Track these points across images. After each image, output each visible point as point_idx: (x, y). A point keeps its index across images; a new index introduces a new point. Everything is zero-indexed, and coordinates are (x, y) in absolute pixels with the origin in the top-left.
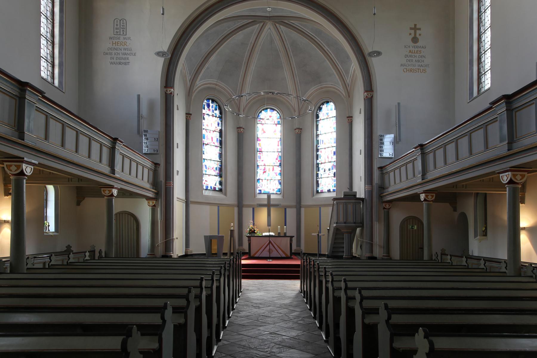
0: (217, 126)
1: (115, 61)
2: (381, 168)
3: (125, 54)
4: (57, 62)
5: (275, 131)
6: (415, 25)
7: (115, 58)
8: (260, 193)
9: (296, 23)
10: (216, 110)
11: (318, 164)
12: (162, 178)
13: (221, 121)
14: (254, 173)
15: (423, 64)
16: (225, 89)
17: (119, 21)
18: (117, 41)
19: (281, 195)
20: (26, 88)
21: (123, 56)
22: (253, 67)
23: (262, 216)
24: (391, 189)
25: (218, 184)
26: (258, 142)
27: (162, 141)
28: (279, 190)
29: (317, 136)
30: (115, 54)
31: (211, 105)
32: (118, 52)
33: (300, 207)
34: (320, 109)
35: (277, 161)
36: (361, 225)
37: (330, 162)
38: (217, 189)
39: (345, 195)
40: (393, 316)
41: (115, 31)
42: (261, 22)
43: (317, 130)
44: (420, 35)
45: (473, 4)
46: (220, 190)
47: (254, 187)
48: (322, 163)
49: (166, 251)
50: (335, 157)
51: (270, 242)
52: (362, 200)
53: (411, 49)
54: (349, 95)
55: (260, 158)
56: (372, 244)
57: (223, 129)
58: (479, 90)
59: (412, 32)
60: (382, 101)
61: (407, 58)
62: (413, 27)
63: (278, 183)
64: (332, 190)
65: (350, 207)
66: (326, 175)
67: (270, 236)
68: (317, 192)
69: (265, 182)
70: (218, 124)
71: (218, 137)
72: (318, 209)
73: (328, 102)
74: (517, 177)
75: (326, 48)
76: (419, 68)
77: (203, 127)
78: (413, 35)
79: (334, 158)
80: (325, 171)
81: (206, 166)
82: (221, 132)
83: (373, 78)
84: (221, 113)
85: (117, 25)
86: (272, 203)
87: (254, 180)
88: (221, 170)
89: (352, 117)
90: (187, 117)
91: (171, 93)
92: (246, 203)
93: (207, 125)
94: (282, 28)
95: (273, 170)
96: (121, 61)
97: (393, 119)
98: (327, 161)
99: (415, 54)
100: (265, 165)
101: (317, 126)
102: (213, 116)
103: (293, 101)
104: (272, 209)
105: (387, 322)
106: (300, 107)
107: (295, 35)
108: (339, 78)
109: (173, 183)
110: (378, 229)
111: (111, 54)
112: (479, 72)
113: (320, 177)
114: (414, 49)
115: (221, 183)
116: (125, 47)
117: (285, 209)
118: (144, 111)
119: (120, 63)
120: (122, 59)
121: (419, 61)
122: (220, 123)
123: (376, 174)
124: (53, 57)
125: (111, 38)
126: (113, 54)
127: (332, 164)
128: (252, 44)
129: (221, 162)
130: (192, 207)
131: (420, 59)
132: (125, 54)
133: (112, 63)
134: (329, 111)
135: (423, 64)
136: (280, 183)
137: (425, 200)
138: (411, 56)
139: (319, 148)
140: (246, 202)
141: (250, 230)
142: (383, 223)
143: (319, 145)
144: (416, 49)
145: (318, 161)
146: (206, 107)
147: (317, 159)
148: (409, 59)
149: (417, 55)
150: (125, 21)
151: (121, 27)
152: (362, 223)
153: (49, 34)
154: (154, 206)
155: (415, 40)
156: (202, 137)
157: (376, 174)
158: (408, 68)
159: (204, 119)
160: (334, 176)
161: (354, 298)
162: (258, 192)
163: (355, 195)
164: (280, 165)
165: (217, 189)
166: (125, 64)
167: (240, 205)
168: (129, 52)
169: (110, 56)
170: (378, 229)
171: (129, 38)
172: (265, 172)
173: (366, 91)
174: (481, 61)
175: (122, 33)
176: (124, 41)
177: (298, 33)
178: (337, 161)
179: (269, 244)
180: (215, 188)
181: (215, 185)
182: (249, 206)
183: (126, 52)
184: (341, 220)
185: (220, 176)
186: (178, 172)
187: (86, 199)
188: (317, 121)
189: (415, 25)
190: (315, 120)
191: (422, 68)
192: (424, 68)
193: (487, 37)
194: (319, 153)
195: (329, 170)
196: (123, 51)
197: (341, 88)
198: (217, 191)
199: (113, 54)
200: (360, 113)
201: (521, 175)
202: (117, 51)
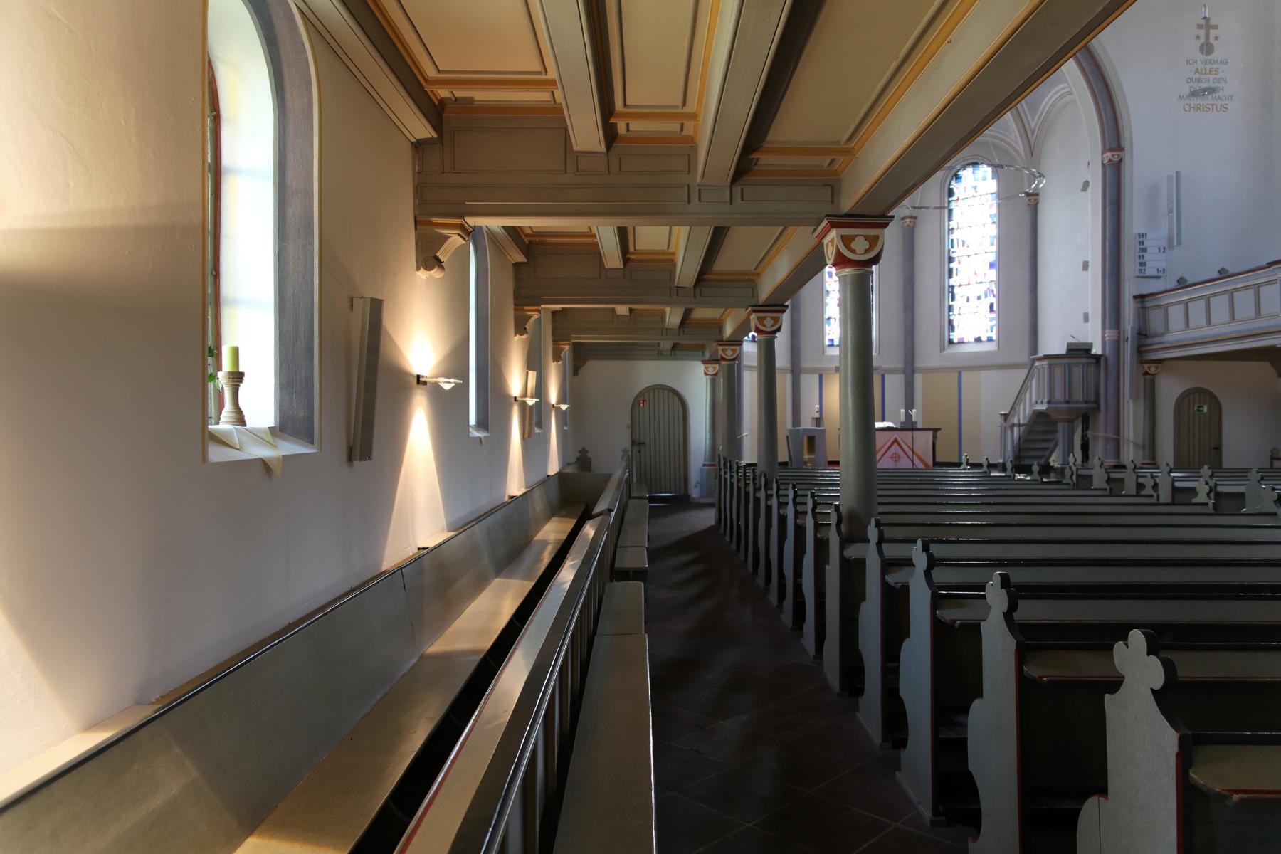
2: (1141, 298)
24: (1170, 338)
29: (951, 230)
33: (913, 372)
39: (1069, 350)
40: (1021, 603)
44: (1216, 38)
51: (896, 441)
53: (1200, 66)
56: (1118, 441)
59: (1202, 32)
60: (1144, 167)
64: (984, 339)
65: (1077, 372)
67: (889, 429)
68: (951, 342)
72: (956, 375)
73: (975, 164)
74: (853, 245)
78: (1202, 40)
79: (993, 274)
83: (1124, 124)
105: (1008, 616)
110: (1132, 416)
113: (956, 310)
127: (984, 287)
139: (953, 255)
140: (806, 363)
142: (1142, 402)
144: (1208, 67)
145: (952, 282)
147: (950, 276)
149: (1211, 77)
155: (1207, 48)
161: (908, 563)
162: (827, 343)
170: (1132, 416)
182: (812, 371)
184: (1059, 395)
187: (589, 362)
194: (952, 265)
195: (979, 298)
201: (866, 237)
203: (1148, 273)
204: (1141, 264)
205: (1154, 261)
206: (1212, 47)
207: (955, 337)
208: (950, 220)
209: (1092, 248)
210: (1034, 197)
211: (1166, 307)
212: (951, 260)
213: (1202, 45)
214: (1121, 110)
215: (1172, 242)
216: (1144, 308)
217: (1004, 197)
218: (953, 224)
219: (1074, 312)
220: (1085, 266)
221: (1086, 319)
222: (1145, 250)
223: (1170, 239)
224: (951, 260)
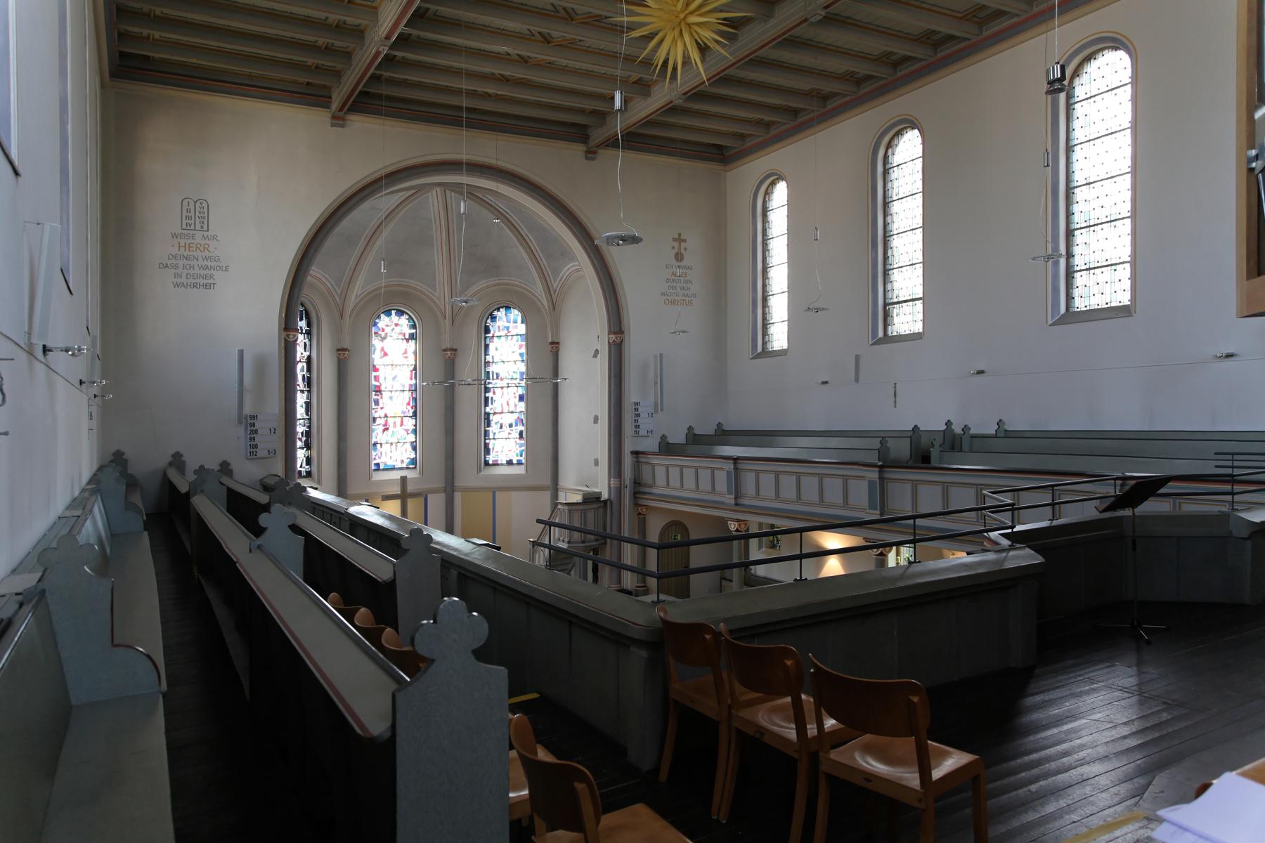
1: (184, 280)
2: (636, 453)
5: (406, 352)
7: (184, 276)
9: (491, 199)
14: (369, 432)
18: (188, 242)
21: (202, 272)
26: (374, 374)
27: (281, 431)
28: (413, 461)
29: (487, 363)
32: (192, 263)
41: (185, 222)
55: (377, 403)
58: (764, 343)
59: (676, 244)
65: (590, 515)
68: (487, 463)
69: (386, 448)
73: (507, 308)
75: (525, 231)
85: (188, 211)
86: (410, 488)
87: (369, 445)
98: (506, 410)
101: (487, 346)
111: (176, 267)
112: (764, 319)
116: (207, 253)
123: (628, 461)
125: (174, 236)
127: (515, 416)
133: (177, 285)
136: (414, 448)
145: (488, 409)
147: (486, 405)
150: (205, 204)
151: (196, 216)
155: (679, 257)
157: (628, 461)
164: (415, 414)
166: (206, 286)
168: (214, 264)
169: (173, 271)
171: (215, 238)
175: (198, 227)
176: (203, 242)
183: (209, 263)
194: (490, 395)
196: (201, 262)
197: (539, 290)
206: (682, 256)
207: (491, 459)
208: (486, 354)
209: (601, 407)
210: (555, 345)
211: (653, 466)
212: (487, 390)
215: (658, 407)
216: (638, 462)
217: (529, 338)
218: (489, 358)
219: (586, 467)
220: (596, 420)
221: (596, 463)
222: (638, 415)
223: (656, 404)
224: (487, 390)
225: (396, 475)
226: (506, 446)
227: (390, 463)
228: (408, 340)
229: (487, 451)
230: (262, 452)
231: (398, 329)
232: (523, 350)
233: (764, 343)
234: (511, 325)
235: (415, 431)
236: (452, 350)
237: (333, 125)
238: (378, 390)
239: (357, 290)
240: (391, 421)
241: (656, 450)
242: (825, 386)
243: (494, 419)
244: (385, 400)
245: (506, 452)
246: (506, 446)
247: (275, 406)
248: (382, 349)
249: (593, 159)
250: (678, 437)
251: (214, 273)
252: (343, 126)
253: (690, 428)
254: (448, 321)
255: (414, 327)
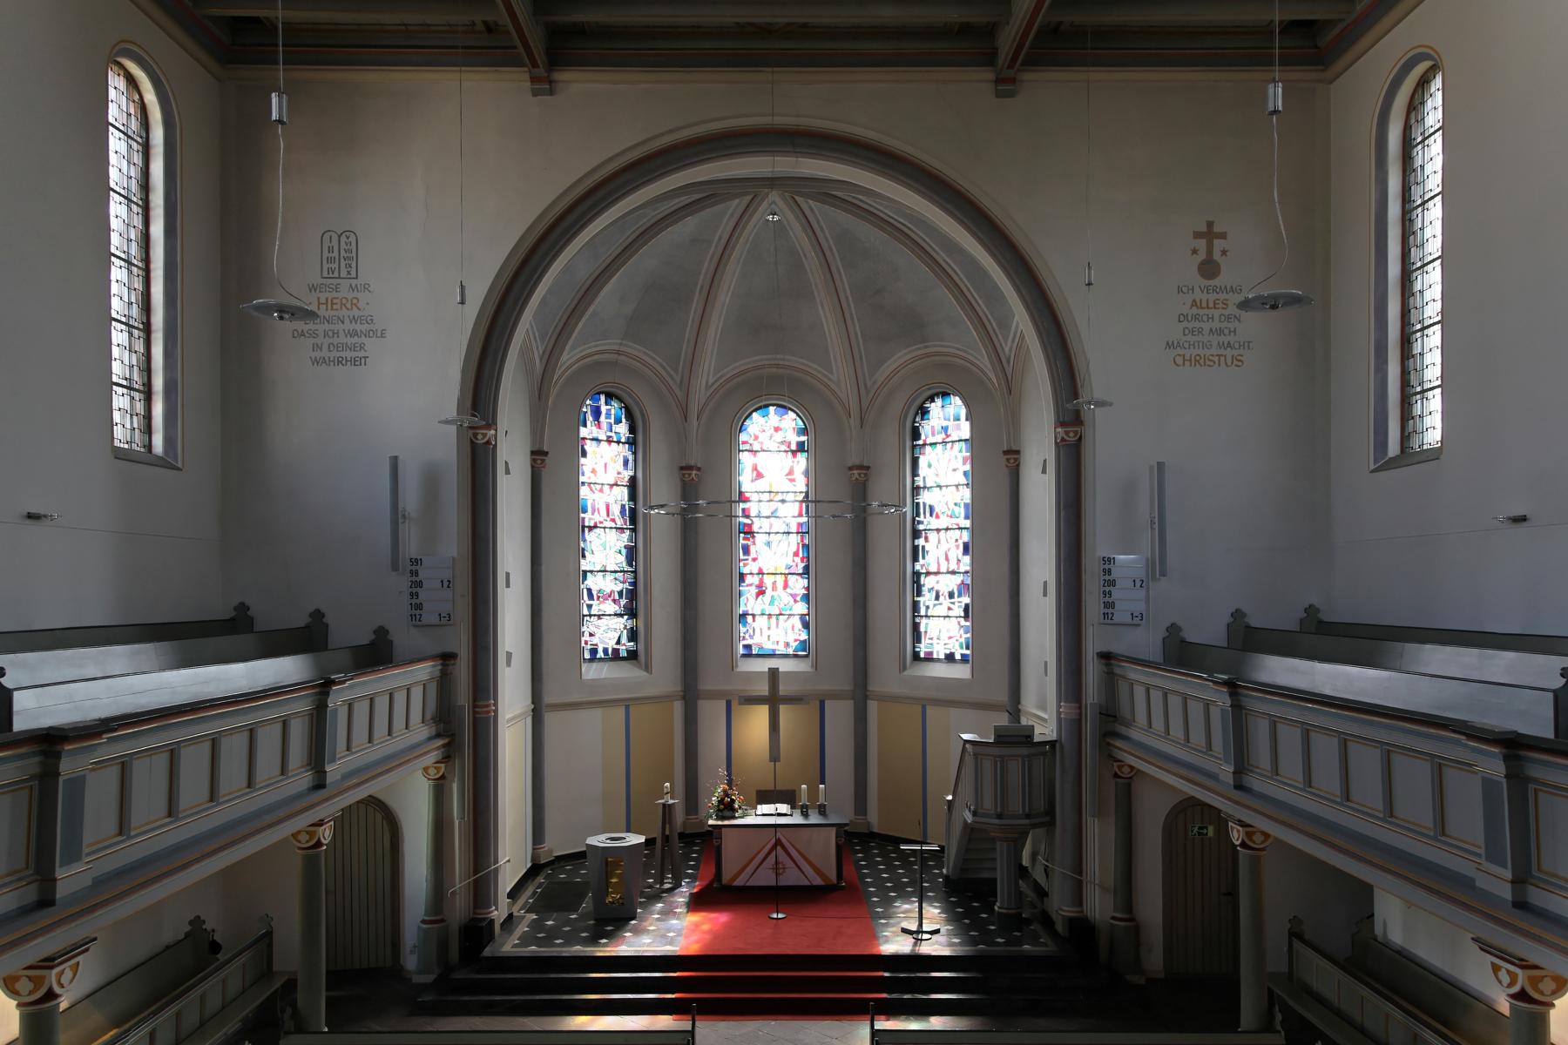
0: (621, 468)
1: (325, 353)
2: (1106, 657)
3: (355, 334)
4: (158, 383)
5: (791, 472)
6: (1210, 224)
7: (325, 347)
8: (748, 655)
10: (618, 421)
11: (917, 575)
12: (463, 696)
13: (635, 453)
14: (732, 597)
15: (1232, 339)
16: (644, 363)
17: (335, 237)
18: (330, 296)
19: (809, 661)
20: (58, 748)
21: (350, 341)
22: (725, 298)
23: (755, 726)
25: (624, 640)
27: (463, 586)
28: (804, 645)
29: (916, 490)
30: (326, 335)
31: (604, 409)
33: (866, 698)
34: (924, 412)
35: (798, 560)
36: (1047, 819)
37: (953, 573)
38: (623, 654)
42: (747, 193)
43: (915, 473)
44: (1224, 253)
45: (1386, 173)
46: (633, 655)
47: (730, 638)
48: (928, 574)
49: (475, 907)
50: (967, 559)
51: (778, 842)
52: (1052, 743)
53: (1198, 295)
54: (1011, 386)
55: (746, 550)
57: (640, 475)
58: (1405, 437)
59: (1202, 244)
60: (1113, 450)
61: (1185, 324)
62: (1204, 229)
63: (799, 625)
64: (958, 657)
65: (1014, 768)
66: (941, 610)
68: (916, 656)
69: (761, 622)
70: (626, 462)
71: (625, 501)
72: (920, 709)
73: (945, 395)
74: (1541, 986)
76: (1222, 352)
77: (582, 479)
78: (1202, 255)
80: (937, 598)
81: (589, 590)
82: (632, 484)
84: (632, 429)
85: (331, 250)
86: (783, 689)
87: (734, 619)
88: (632, 594)
89: (1018, 452)
90: (534, 461)
91: (488, 442)
92: (708, 687)
93: (594, 471)
94: (813, 207)
95: (786, 586)
96: (343, 354)
97: (1144, 506)
98: (943, 569)
99: (1210, 312)
100: (761, 572)
101: (915, 462)
102: (609, 441)
103: (840, 377)
104: (783, 709)
106: (865, 404)
107: (845, 218)
108: (982, 339)
109: (496, 705)
110: (1099, 837)
111: (314, 334)
112: (1405, 383)
113: (923, 612)
114: (1205, 296)
115: (633, 635)
116: (355, 312)
117: (822, 704)
118: (411, 500)
119: (339, 361)
120: (345, 347)
121: (1220, 332)
122: (631, 458)
124: (145, 186)
126: (321, 333)
127: (958, 579)
128: (724, 241)
129: (635, 572)
130: (550, 719)
131: (1222, 325)
132: (355, 334)
133: (316, 361)
134: (948, 420)
135: (1232, 339)
136: (806, 625)
137: (1243, 845)
138: (1196, 318)
140: (705, 684)
141: (721, 802)
143: (922, 518)
145: (918, 567)
146: (590, 418)
147: (915, 559)
148: (1191, 325)
149: (1216, 313)
151: (342, 255)
152: (1051, 812)
153: (134, 245)
154: (443, 777)
155: (1209, 268)
156: (576, 506)
158: (1187, 353)
159: (584, 454)
160: (966, 617)
162: (741, 651)
163: (1031, 736)
164: (806, 570)
165: (623, 654)
166: (355, 362)
167: (690, 694)
168: (365, 327)
169: (312, 341)
170: (1099, 837)
171: (366, 287)
172: (761, 593)
173: (1061, 423)
174: (1410, 349)
175: (344, 274)
177: (858, 216)
178: (974, 572)
179: (774, 847)
180: (616, 651)
181: (618, 642)
182: (714, 695)
183: (358, 327)
184: (988, 804)
185: (631, 612)
186: (509, 655)
188: (914, 447)
189: (1210, 224)
190: (908, 444)
191: (1229, 352)
192: (1235, 352)
193: (1431, 284)
194: (921, 542)
195: (951, 595)
196: (348, 326)
197: (985, 363)
198: (623, 659)
199: (321, 333)
200: (1044, 471)
202: (332, 327)
203: (1117, 619)
204: (1107, 605)
205: (1128, 601)
212: (916, 534)
213: (1203, 263)
214: (1079, 363)
215: (1157, 568)
224: (916, 534)
225: (763, 666)
226: (945, 633)
227: (769, 646)
228: (794, 453)
229: (917, 637)
230: (429, 617)
231: (779, 436)
232: (968, 467)
233: (1405, 437)
234: (951, 424)
235: (806, 598)
236: (860, 467)
237: (535, 93)
238: (749, 532)
239: (708, 373)
240: (768, 580)
241: (1155, 654)
242: (1521, 529)
243: (927, 582)
244: (758, 546)
245: (944, 636)
246: (945, 633)
247: (452, 545)
248: (755, 468)
249: (1012, 94)
250: (1209, 630)
251: (363, 339)
252: (551, 93)
253: (1238, 615)
254: (854, 421)
255: (804, 431)
